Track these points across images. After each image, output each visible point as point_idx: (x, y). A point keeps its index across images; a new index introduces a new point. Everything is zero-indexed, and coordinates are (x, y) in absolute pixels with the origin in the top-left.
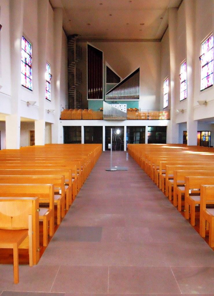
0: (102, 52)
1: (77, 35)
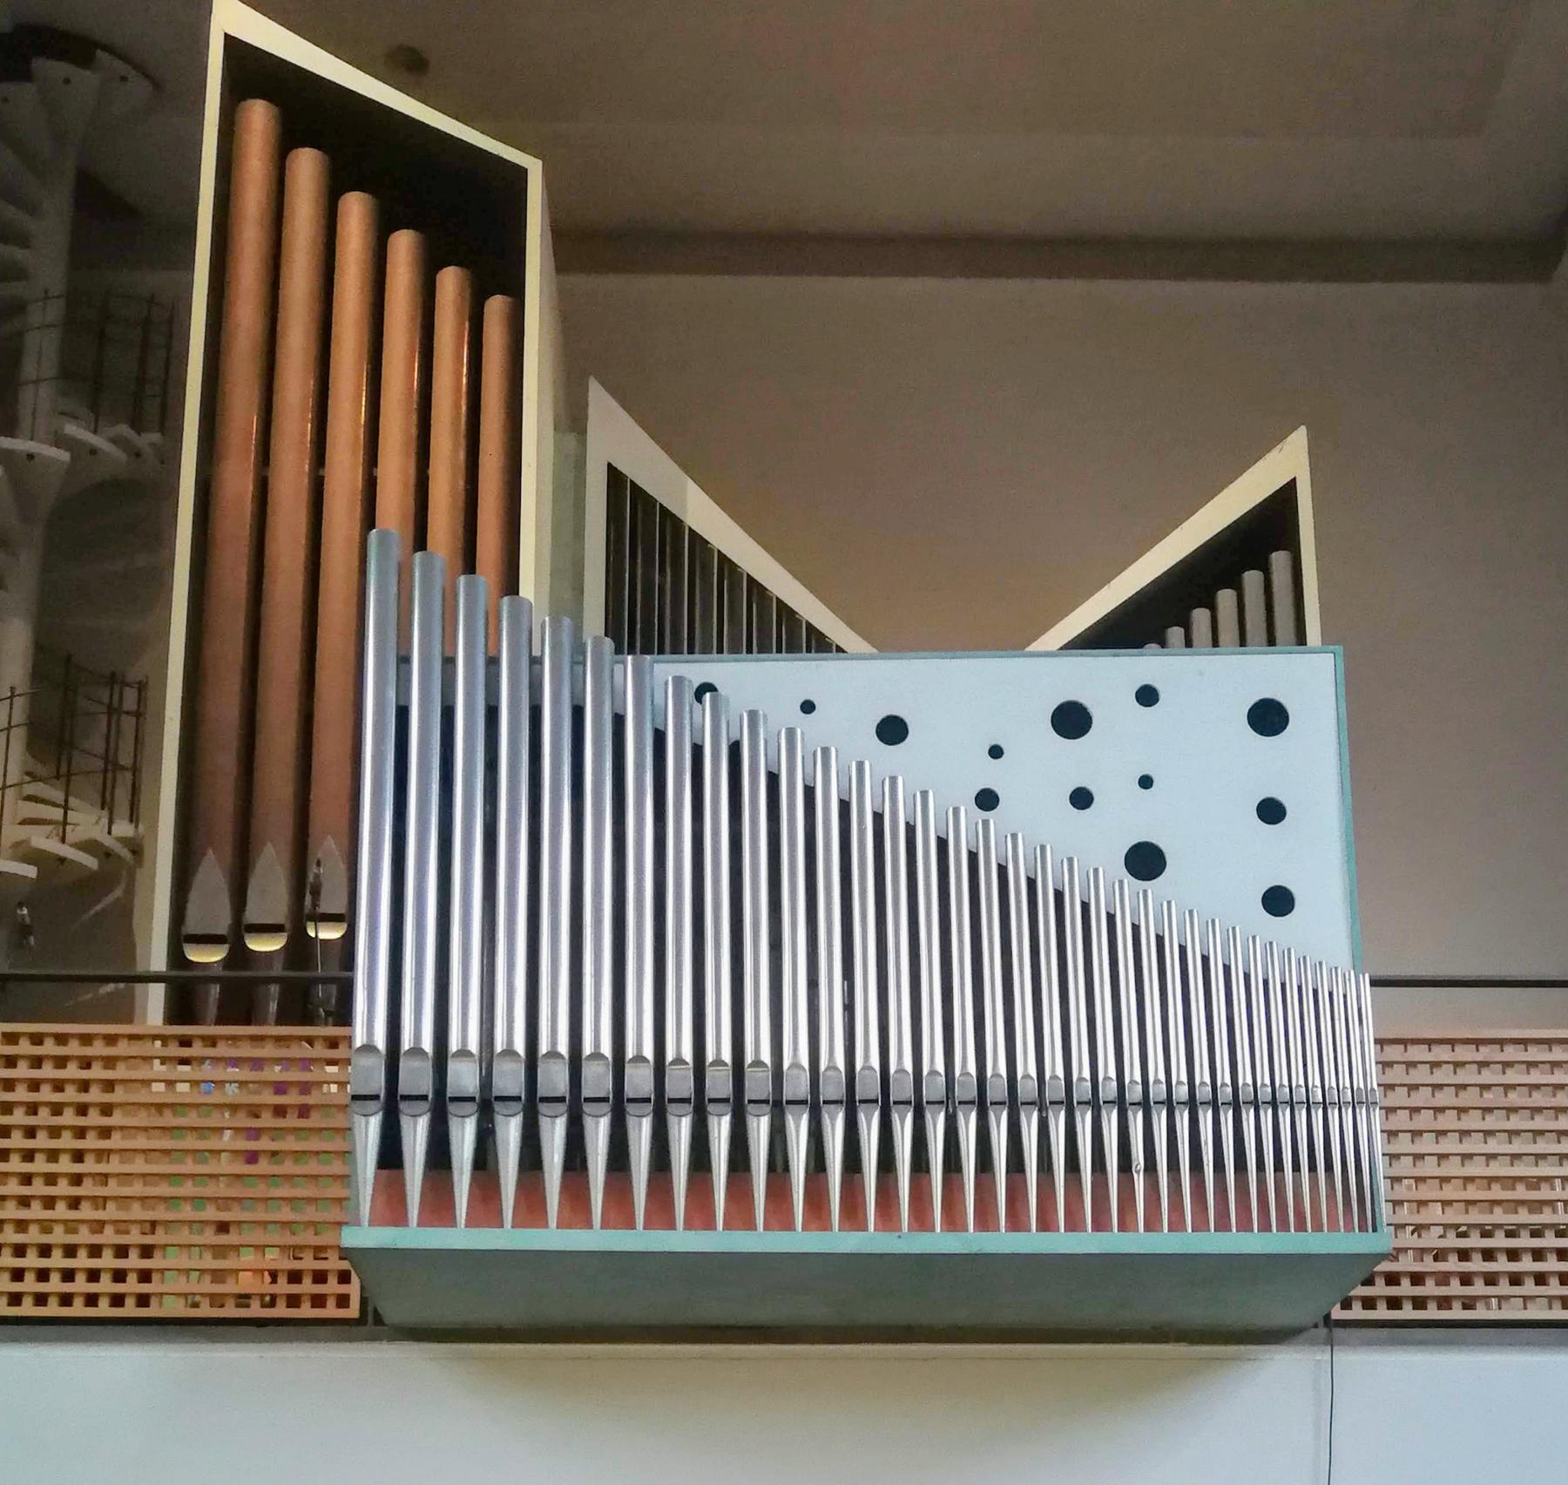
0: (521, 173)
1: (77, 48)
